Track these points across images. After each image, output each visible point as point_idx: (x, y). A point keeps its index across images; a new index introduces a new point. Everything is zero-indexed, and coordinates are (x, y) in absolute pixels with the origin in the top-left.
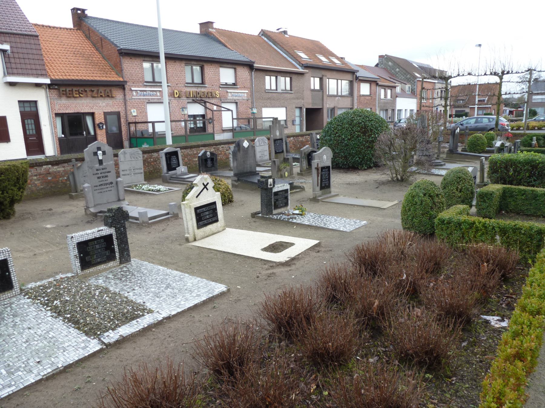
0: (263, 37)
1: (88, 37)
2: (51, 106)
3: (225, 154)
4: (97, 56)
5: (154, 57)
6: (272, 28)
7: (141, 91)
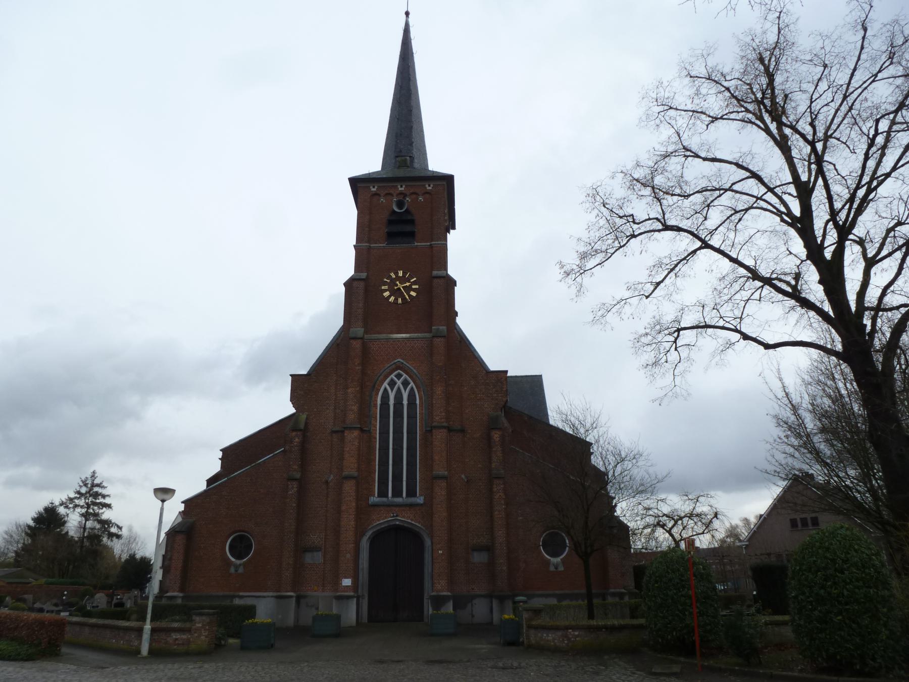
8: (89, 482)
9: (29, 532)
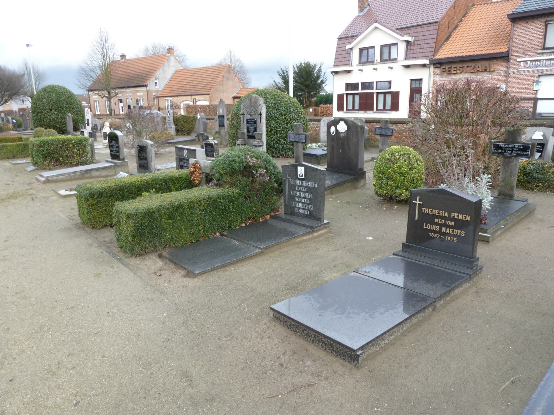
3: (315, 130)
7: (531, 61)
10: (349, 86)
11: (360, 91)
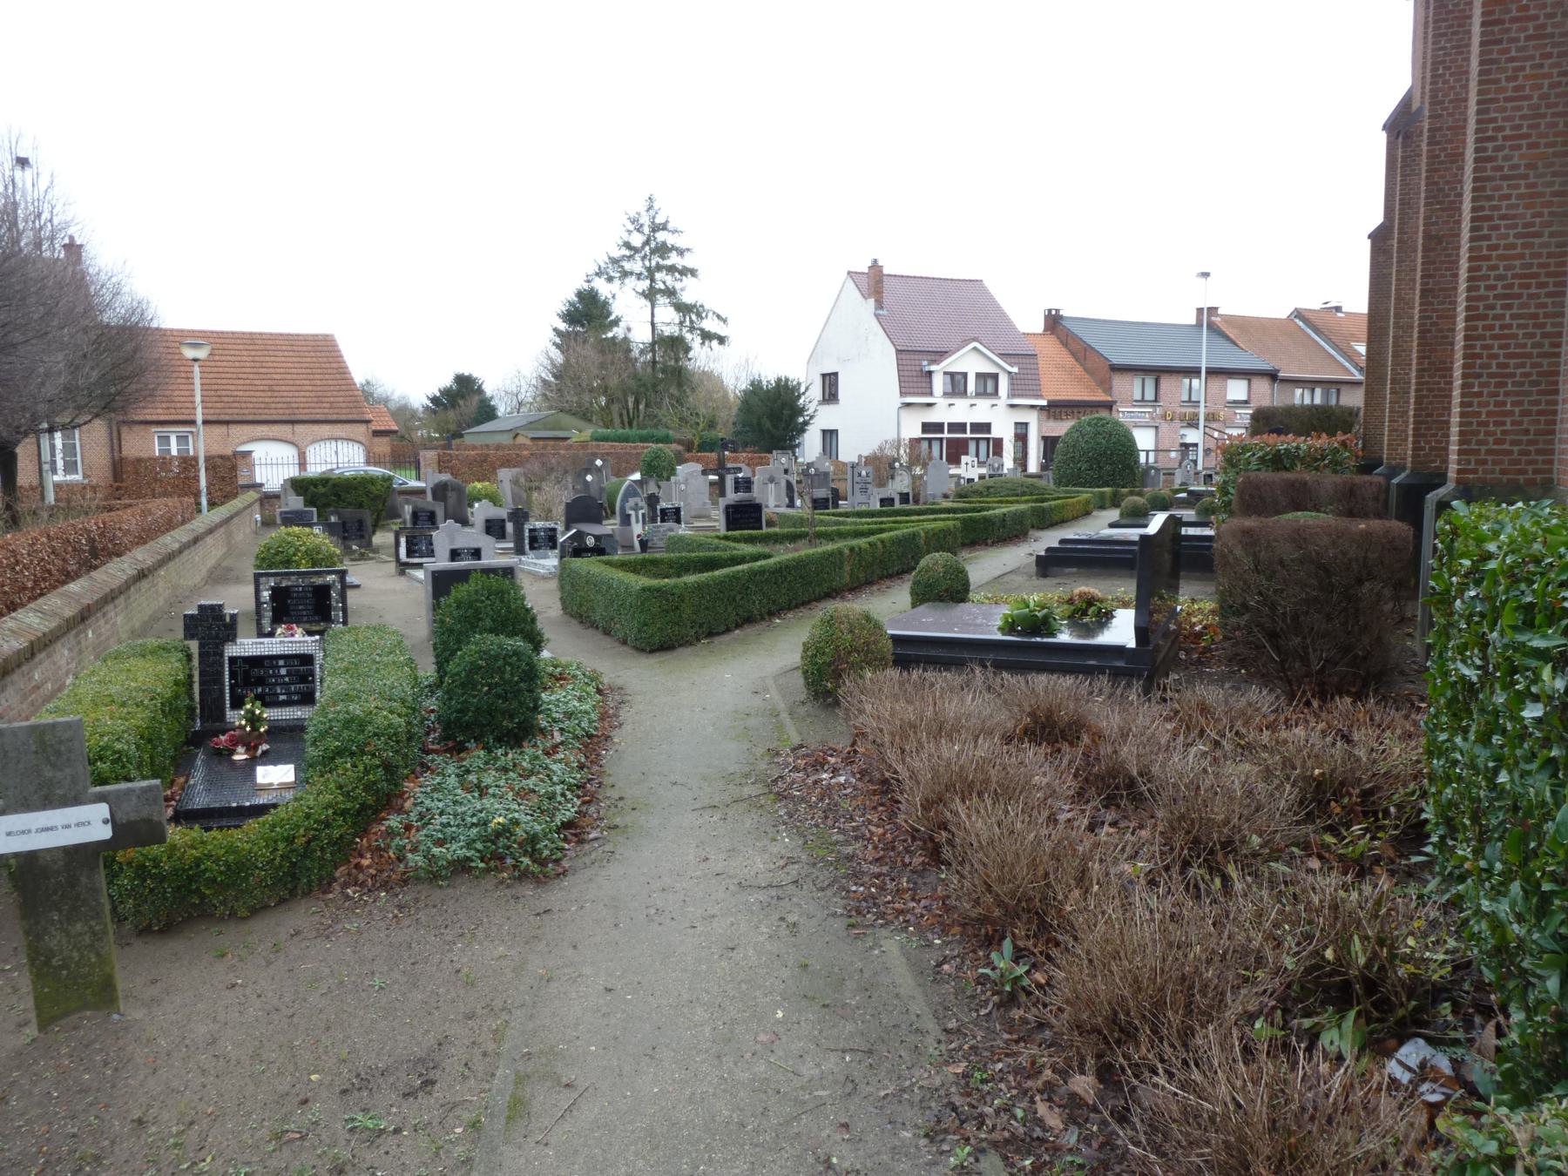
0: (1297, 321)
1: (1065, 344)
2: (1039, 430)
4: (1079, 370)
5: (1193, 372)
6: (1313, 303)
8: (645, 220)
9: (558, 340)
10: (926, 427)
11: (946, 435)
